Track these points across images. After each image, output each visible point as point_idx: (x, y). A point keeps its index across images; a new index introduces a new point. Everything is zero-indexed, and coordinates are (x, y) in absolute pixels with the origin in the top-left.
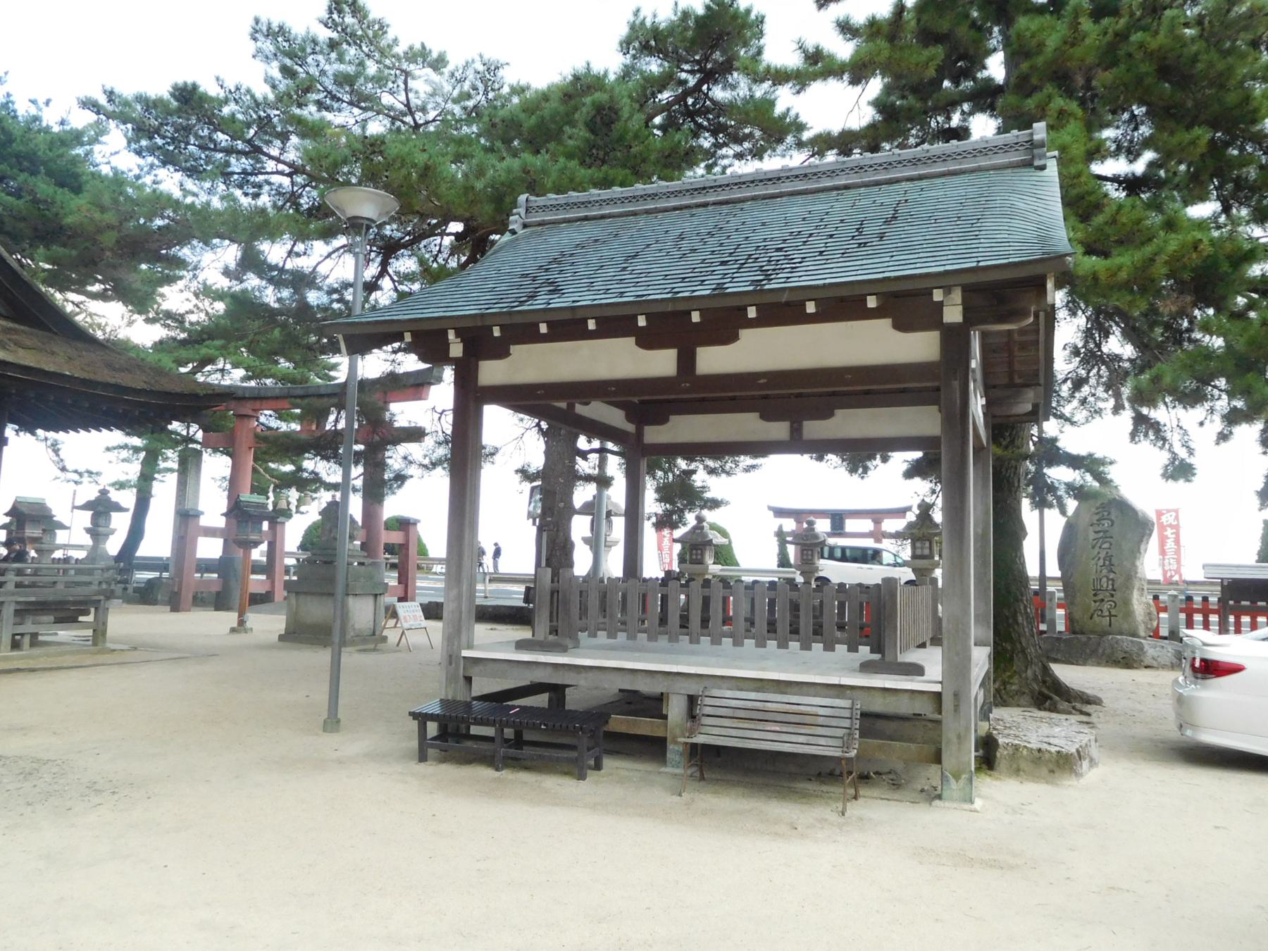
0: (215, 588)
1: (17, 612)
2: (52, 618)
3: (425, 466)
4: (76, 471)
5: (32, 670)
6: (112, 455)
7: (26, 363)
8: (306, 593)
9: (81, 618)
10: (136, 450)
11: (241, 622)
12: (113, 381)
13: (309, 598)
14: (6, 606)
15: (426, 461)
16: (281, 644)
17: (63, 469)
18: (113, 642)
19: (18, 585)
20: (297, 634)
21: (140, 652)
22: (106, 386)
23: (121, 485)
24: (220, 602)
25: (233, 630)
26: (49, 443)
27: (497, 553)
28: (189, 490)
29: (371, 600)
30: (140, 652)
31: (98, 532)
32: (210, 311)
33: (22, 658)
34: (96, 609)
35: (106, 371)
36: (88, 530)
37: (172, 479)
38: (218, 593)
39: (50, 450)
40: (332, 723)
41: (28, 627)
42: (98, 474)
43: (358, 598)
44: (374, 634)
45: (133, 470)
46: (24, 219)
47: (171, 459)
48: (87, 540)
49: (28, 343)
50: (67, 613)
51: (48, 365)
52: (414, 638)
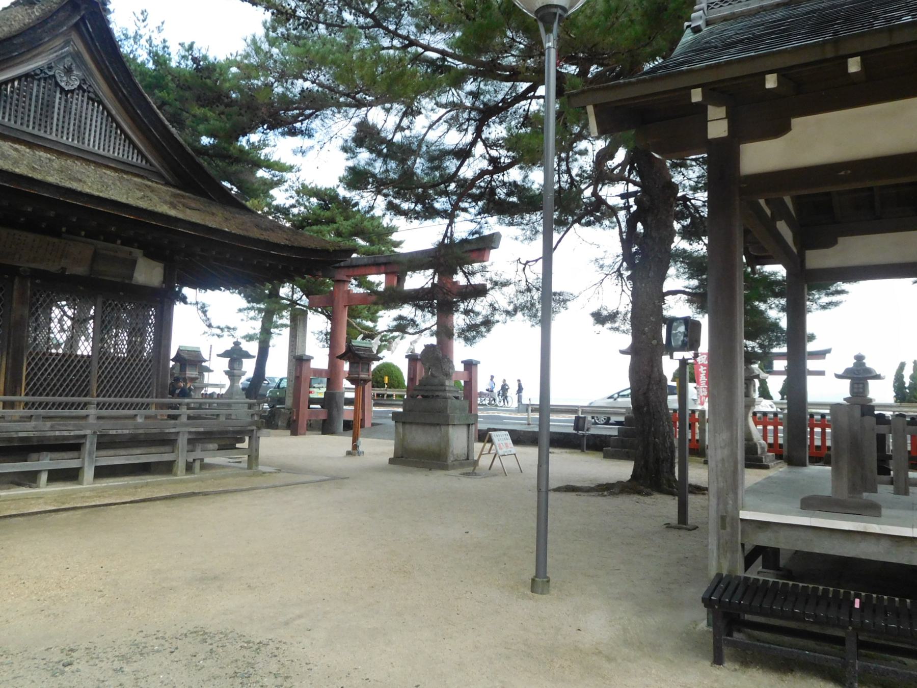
0: (323, 416)
1: (190, 441)
2: (216, 446)
3: (508, 313)
4: (219, 327)
5: (205, 494)
6: (242, 315)
7: (193, 220)
8: (411, 423)
9: (238, 445)
10: (260, 310)
11: (355, 447)
12: (262, 237)
13: (414, 427)
14: (181, 435)
15: (511, 308)
16: (392, 466)
17: (210, 326)
18: (265, 464)
19: (189, 418)
20: (405, 457)
21: (293, 476)
22: (257, 242)
23: (250, 338)
24: (326, 427)
25: (349, 453)
26: (199, 306)
27: (520, 390)
28: (299, 340)
29: (465, 429)
30: (293, 476)
31: (233, 373)
32: (307, 204)
33: (194, 481)
34: (250, 438)
35: (255, 229)
36: (227, 373)
37: (286, 332)
38: (324, 421)
39: (200, 312)
40: (539, 582)
41: (198, 454)
42: (234, 329)
43: (455, 427)
44: (468, 459)
45: (256, 326)
46: (189, 88)
47: (285, 318)
48: (226, 381)
49: (193, 205)
50: (227, 440)
51: (212, 223)
52: (509, 463)
